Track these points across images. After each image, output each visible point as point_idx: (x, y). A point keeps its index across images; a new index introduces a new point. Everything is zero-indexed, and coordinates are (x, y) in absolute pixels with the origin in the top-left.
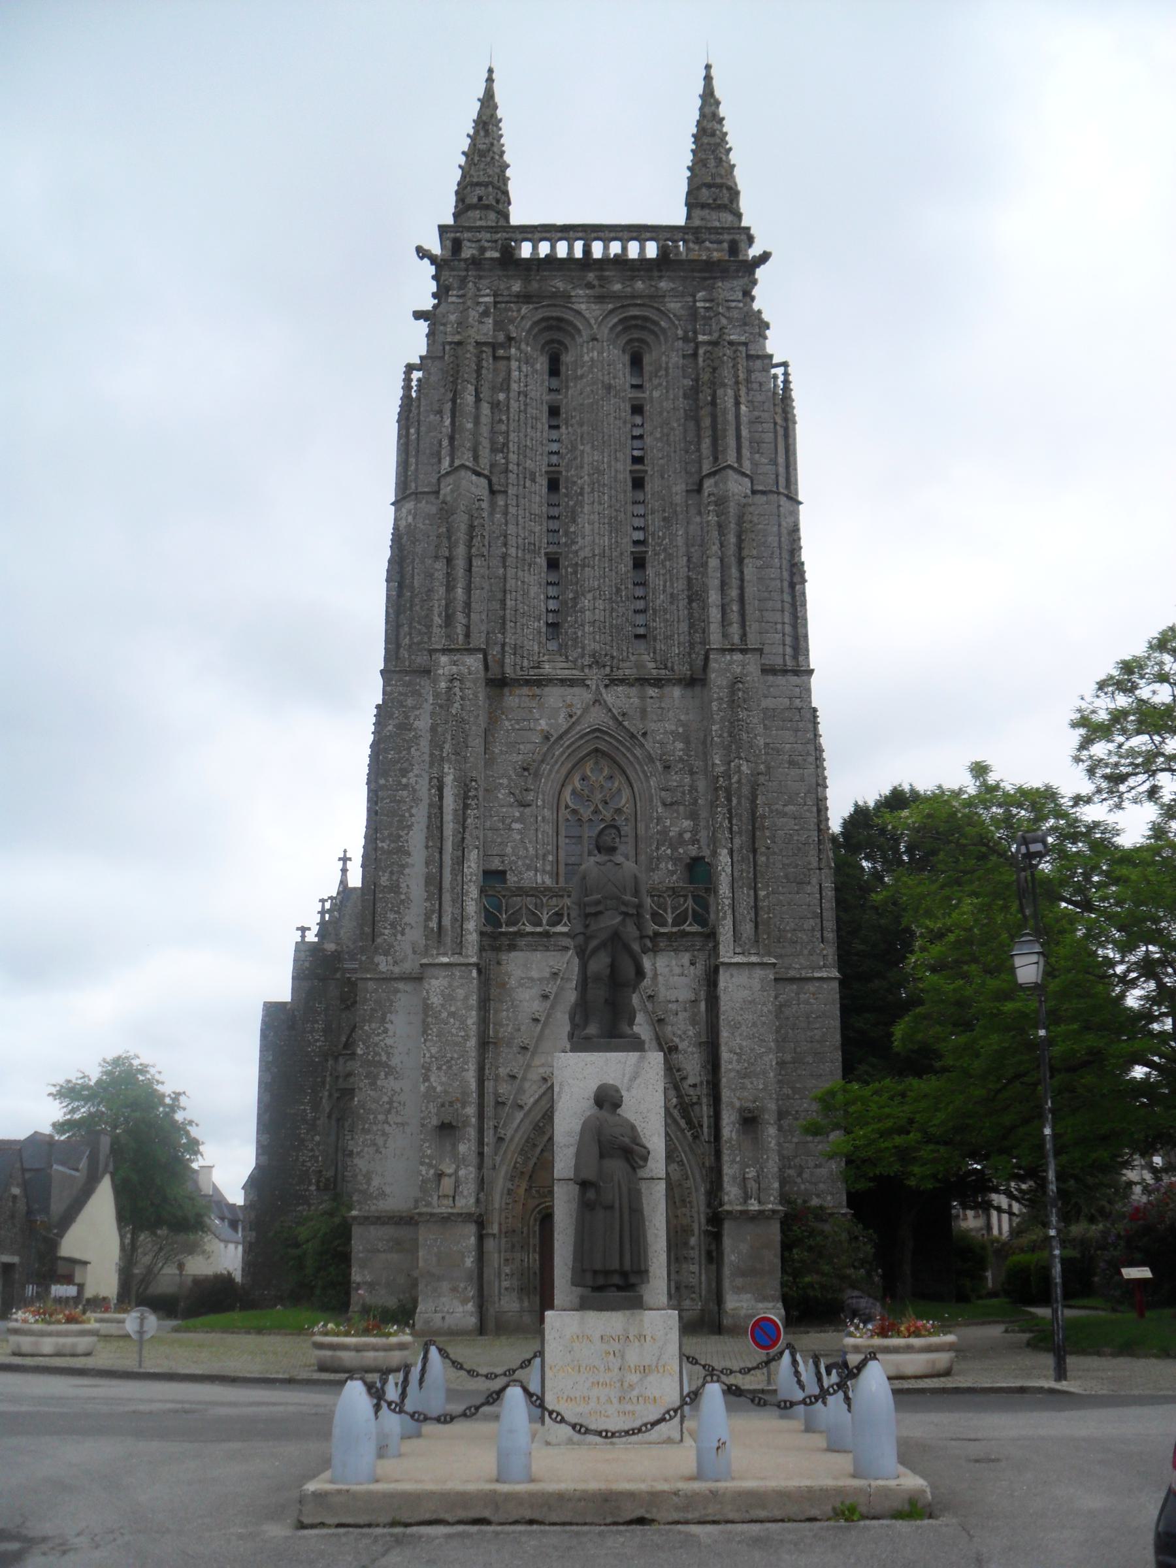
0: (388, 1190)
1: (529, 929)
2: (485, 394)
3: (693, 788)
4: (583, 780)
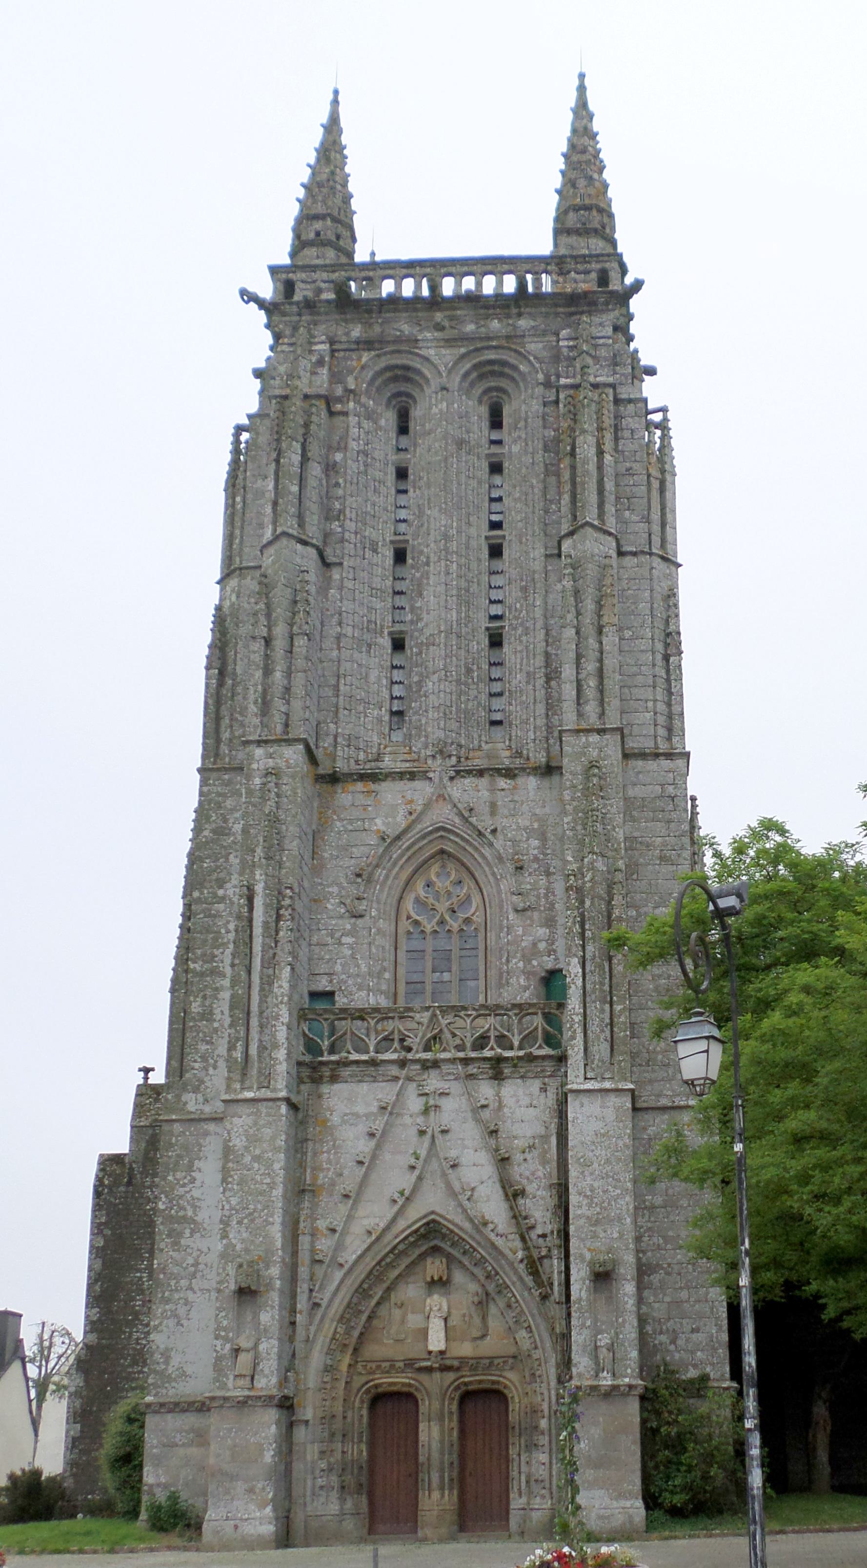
0: (189, 1370)
1: (355, 1056)
2: (314, 450)
3: (549, 891)
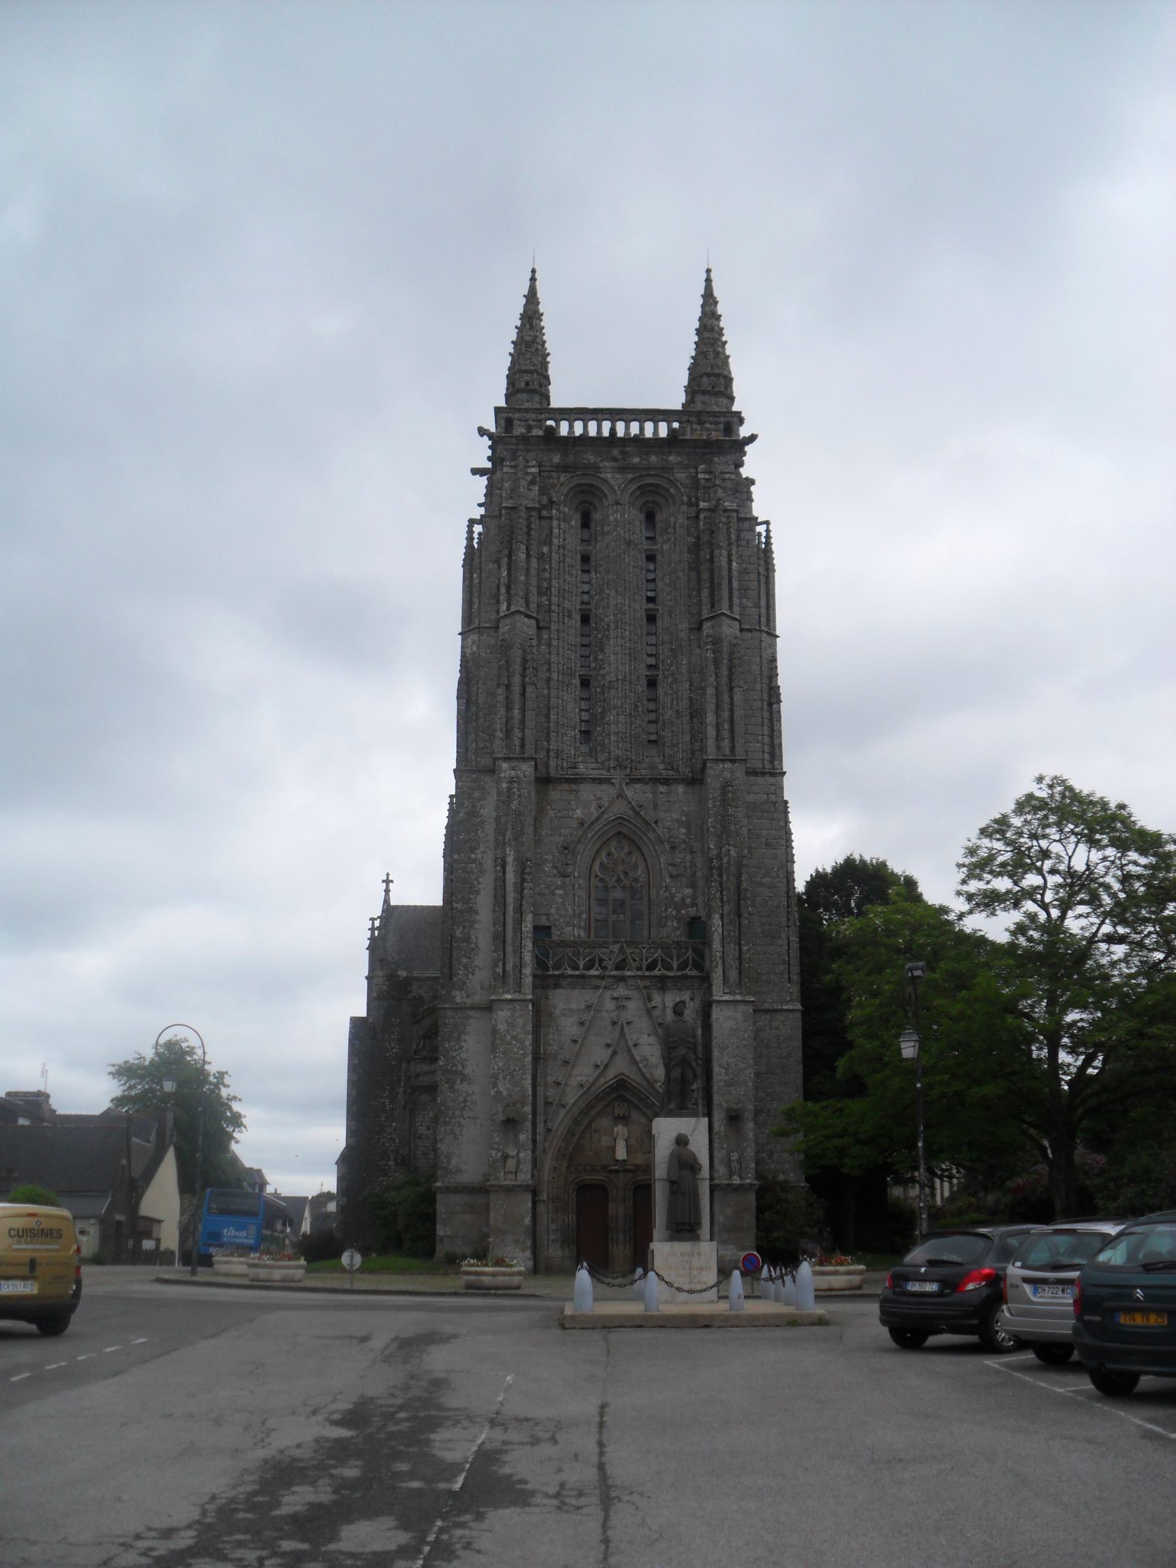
1: (570, 972)
2: (534, 548)
3: (693, 864)
4: (609, 855)
